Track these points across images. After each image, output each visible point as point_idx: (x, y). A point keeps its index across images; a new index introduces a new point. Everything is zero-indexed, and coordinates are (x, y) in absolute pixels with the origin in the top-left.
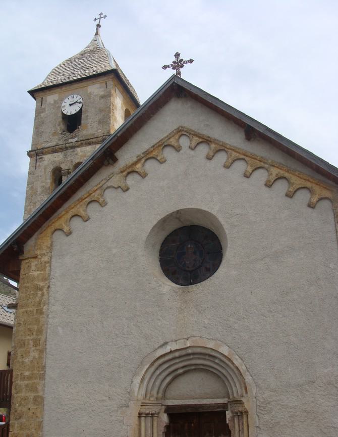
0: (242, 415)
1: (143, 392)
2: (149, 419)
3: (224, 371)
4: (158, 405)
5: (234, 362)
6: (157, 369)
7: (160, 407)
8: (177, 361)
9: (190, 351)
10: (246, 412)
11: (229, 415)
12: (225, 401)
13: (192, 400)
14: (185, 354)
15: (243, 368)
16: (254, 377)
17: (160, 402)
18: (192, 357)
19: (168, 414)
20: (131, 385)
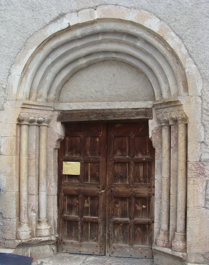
0: (176, 124)
1: (26, 88)
2: (34, 129)
3: (148, 61)
4: (48, 109)
5: (168, 41)
6: (48, 56)
7: (51, 113)
8: (79, 44)
9: (98, 27)
10: (185, 120)
11: (153, 125)
12: (149, 104)
13: (99, 103)
14: (92, 33)
15: (181, 52)
16: (201, 66)
17: (51, 104)
18: (100, 38)
19: (62, 123)
20: (7, 78)
